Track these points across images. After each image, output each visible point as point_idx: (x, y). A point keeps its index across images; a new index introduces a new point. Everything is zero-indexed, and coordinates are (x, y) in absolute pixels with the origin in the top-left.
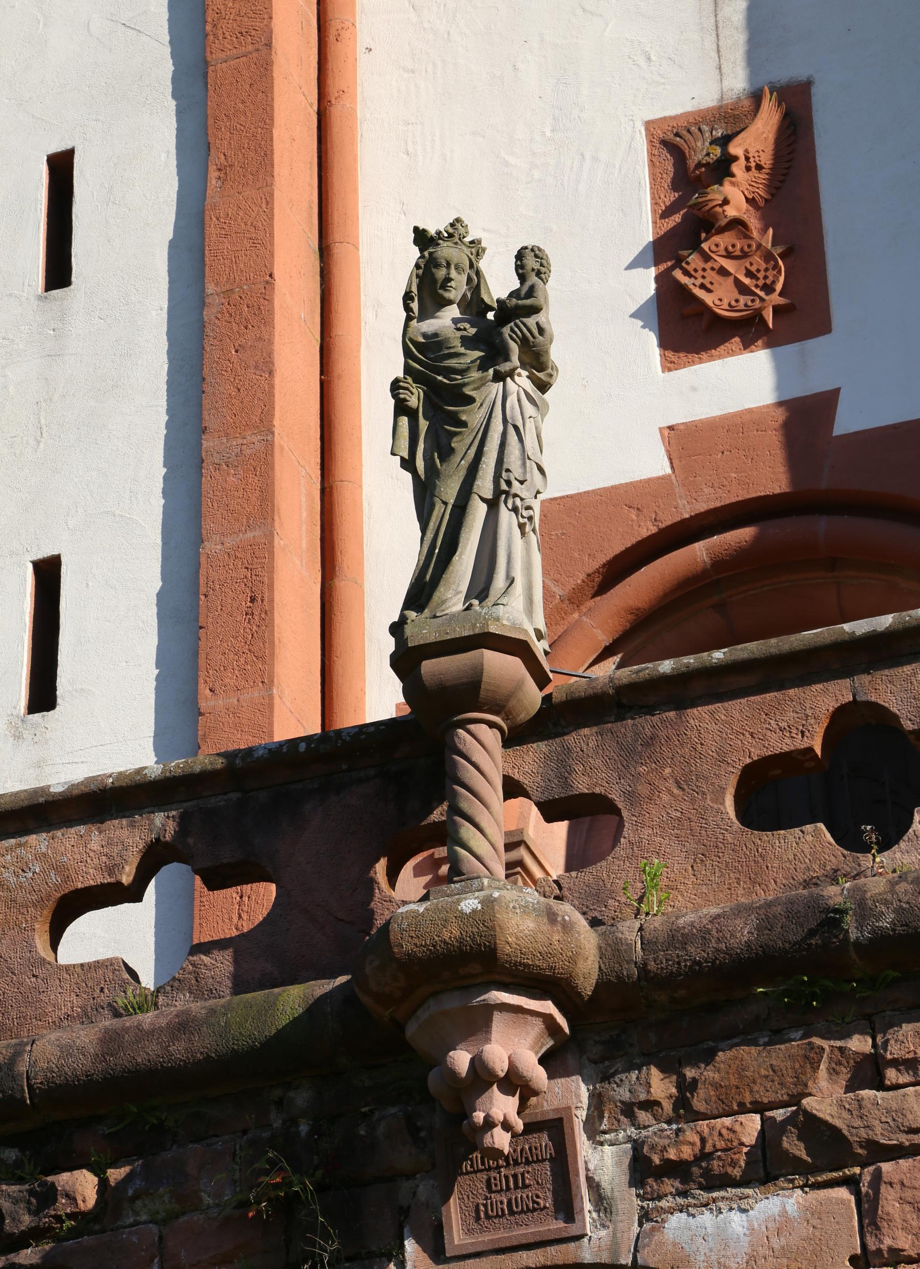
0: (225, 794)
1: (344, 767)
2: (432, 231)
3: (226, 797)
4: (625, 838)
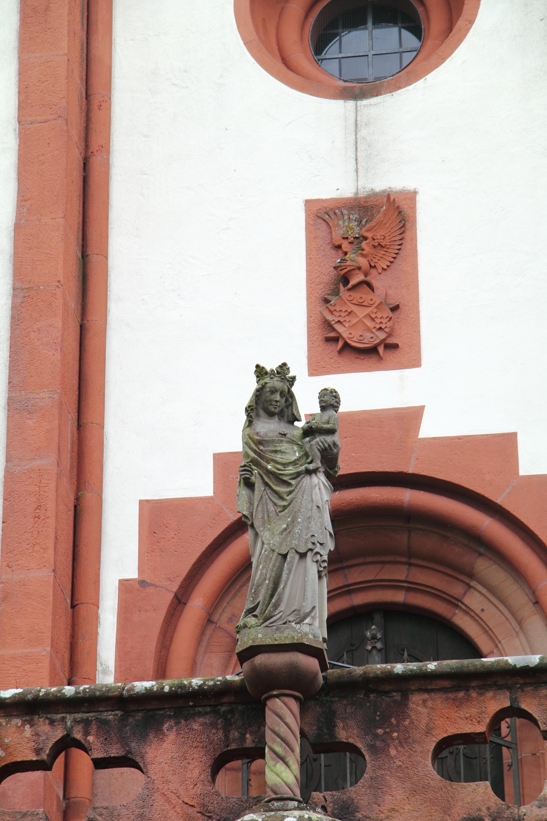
0: (113, 711)
1: (191, 704)
2: (268, 369)
3: (113, 713)
4: (367, 774)
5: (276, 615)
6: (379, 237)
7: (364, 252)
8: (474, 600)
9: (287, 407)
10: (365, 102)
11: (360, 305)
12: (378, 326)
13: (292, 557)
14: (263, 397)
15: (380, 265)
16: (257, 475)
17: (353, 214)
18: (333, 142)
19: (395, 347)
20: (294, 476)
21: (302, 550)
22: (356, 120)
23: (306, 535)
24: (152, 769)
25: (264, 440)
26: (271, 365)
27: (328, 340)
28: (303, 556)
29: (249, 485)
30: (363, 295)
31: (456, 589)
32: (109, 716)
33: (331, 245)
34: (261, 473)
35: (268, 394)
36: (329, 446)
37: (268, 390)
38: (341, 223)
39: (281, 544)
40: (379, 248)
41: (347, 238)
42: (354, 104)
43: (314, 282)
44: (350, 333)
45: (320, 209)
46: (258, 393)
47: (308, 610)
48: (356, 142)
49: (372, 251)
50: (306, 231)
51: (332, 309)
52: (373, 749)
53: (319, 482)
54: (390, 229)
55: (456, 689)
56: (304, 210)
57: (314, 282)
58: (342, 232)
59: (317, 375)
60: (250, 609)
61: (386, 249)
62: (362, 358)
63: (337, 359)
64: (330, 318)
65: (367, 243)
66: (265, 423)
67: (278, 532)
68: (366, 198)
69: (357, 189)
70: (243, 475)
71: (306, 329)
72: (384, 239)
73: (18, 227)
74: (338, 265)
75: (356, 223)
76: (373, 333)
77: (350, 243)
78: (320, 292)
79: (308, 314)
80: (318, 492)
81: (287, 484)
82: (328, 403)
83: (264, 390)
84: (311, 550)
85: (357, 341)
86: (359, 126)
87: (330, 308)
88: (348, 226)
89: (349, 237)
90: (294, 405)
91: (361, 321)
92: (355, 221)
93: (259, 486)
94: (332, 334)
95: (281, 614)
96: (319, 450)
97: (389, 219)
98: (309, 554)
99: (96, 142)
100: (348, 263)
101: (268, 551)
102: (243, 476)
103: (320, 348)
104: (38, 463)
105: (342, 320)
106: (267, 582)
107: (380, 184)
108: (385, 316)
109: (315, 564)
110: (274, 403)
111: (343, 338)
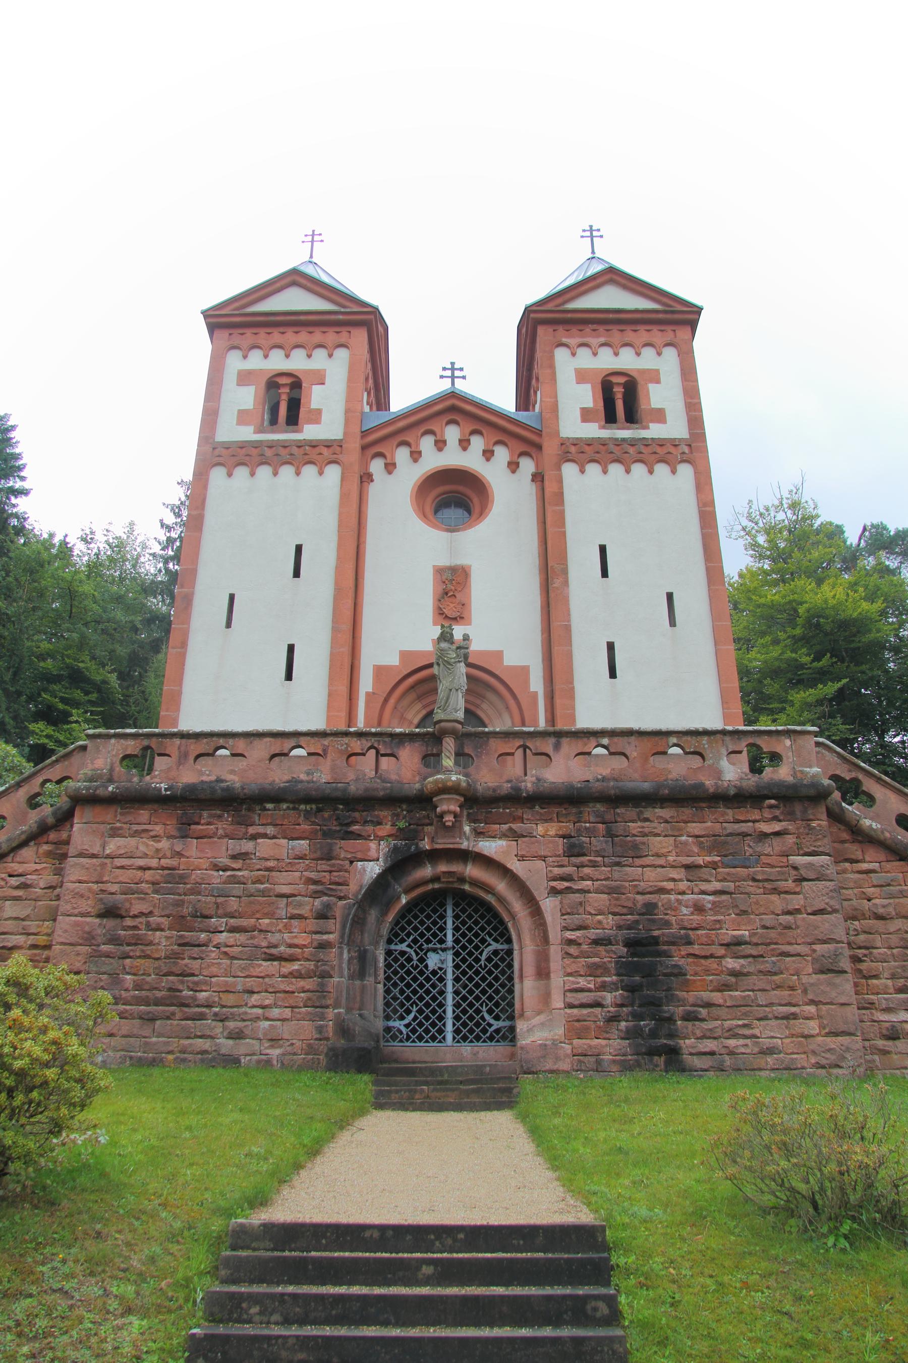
8: (484, 706)
24: (401, 759)
28: (457, 690)
31: (478, 702)
32: (387, 739)
52: (476, 755)
53: (462, 664)
55: (505, 737)
73: (337, 568)
80: (462, 668)
88: (448, 575)
93: (442, 665)
99: (362, 540)
104: (342, 650)
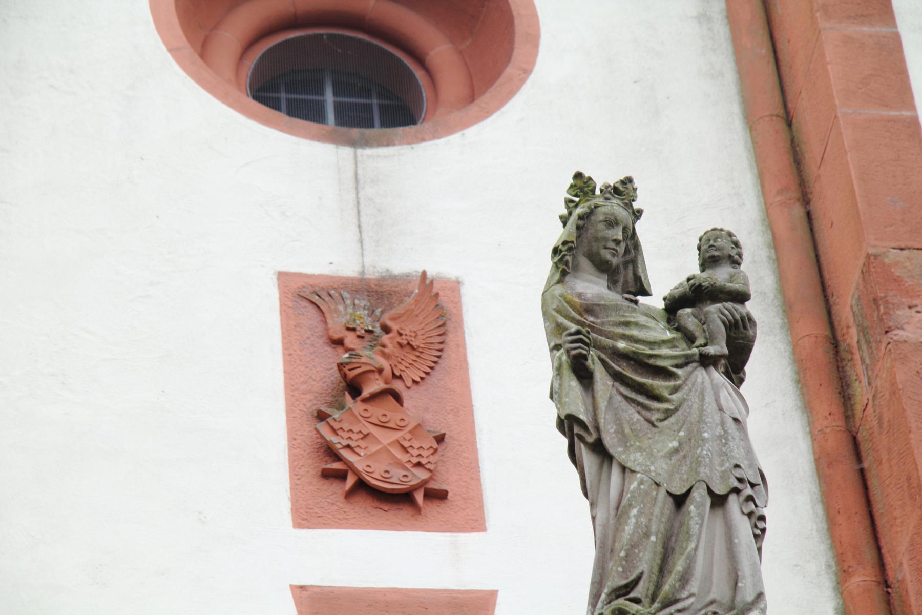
5: (684, 599)
6: (408, 332)
7: (386, 350)
9: (626, 264)
10: (368, 151)
11: (382, 426)
12: (415, 460)
13: (700, 498)
14: (591, 231)
15: (409, 376)
16: (596, 358)
17: (359, 300)
18: (320, 198)
19: (439, 496)
20: (679, 361)
21: (719, 490)
22: (356, 174)
23: (722, 465)
25: (599, 305)
26: (603, 176)
27: (327, 475)
28: (719, 501)
29: (584, 375)
30: (385, 410)
33: (324, 338)
34: (603, 356)
35: (601, 226)
36: (742, 318)
37: (602, 218)
38: (341, 308)
39: (671, 475)
40: (407, 349)
41: (354, 330)
42: (352, 155)
43: (297, 389)
44: (369, 466)
45: (303, 287)
46: (581, 223)
47: (750, 598)
48: (358, 203)
49: (397, 351)
50: (281, 314)
51: (336, 426)
54: (423, 325)
56: (276, 286)
57: (297, 389)
58: (344, 321)
59: (309, 528)
60: (620, 588)
61: (418, 354)
62: (386, 508)
63: (341, 505)
64: (333, 439)
65: (391, 338)
66: (590, 282)
67: (661, 453)
68: (378, 280)
69: (363, 266)
70: (575, 349)
71: (287, 457)
72: (415, 337)
74: (347, 360)
75: (366, 312)
76: (407, 470)
77: (359, 337)
78: (309, 405)
79: (289, 434)
81: (665, 373)
82: (726, 252)
83: (593, 218)
84: (736, 491)
85: (380, 478)
86: (361, 182)
87: (332, 423)
89: (358, 328)
90: (640, 262)
91: (385, 449)
92: (364, 309)
93: (602, 380)
94: (336, 466)
95: (692, 600)
96: (724, 323)
97: (423, 310)
98: (733, 498)
100: (363, 360)
101: (647, 484)
102: (574, 352)
103: (311, 487)
105: (353, 444)
106: (653, 538)
107: (402, 260)
108: (426, 446)
109: (746, 518)
110: (611, 245)
111: (356, 472)
